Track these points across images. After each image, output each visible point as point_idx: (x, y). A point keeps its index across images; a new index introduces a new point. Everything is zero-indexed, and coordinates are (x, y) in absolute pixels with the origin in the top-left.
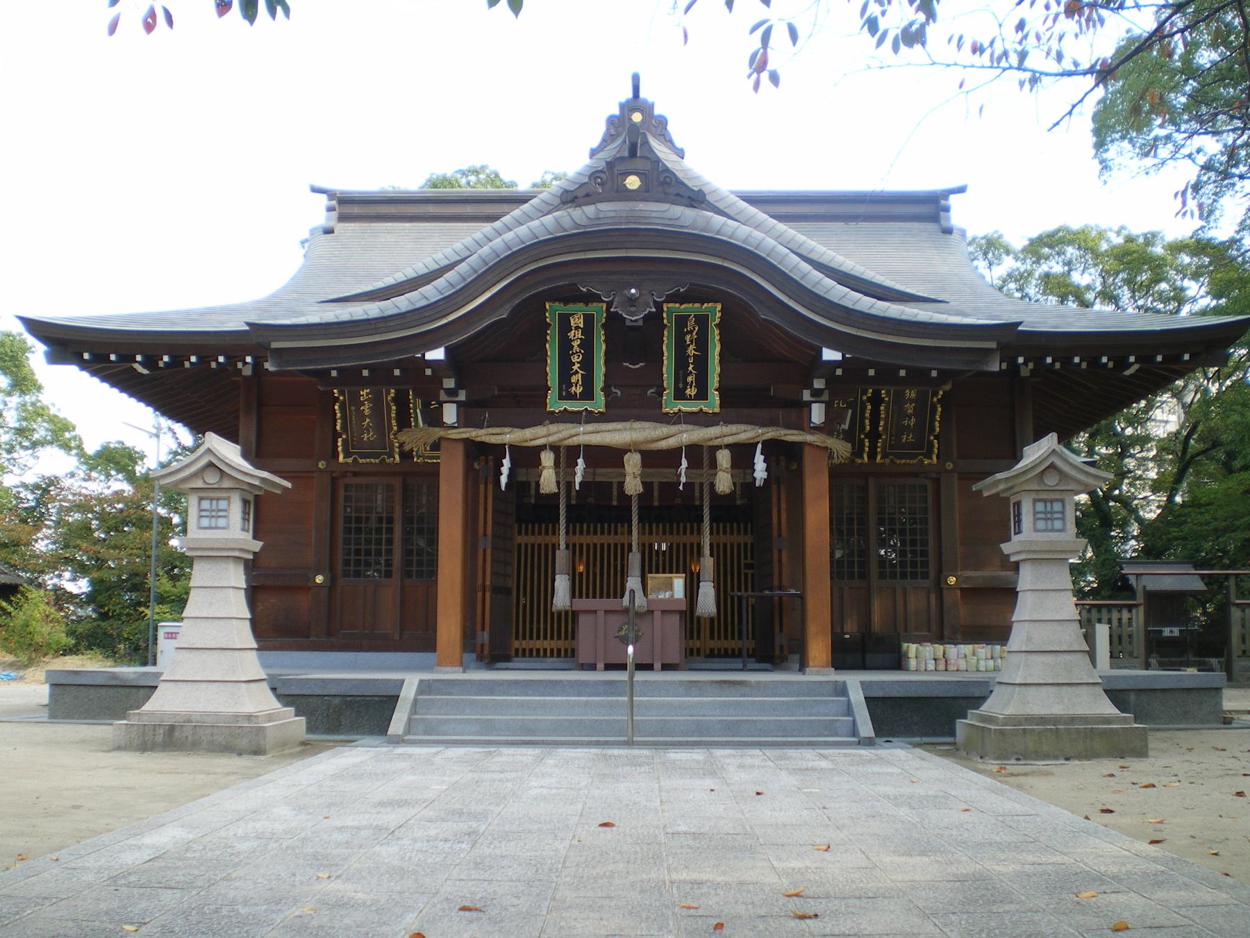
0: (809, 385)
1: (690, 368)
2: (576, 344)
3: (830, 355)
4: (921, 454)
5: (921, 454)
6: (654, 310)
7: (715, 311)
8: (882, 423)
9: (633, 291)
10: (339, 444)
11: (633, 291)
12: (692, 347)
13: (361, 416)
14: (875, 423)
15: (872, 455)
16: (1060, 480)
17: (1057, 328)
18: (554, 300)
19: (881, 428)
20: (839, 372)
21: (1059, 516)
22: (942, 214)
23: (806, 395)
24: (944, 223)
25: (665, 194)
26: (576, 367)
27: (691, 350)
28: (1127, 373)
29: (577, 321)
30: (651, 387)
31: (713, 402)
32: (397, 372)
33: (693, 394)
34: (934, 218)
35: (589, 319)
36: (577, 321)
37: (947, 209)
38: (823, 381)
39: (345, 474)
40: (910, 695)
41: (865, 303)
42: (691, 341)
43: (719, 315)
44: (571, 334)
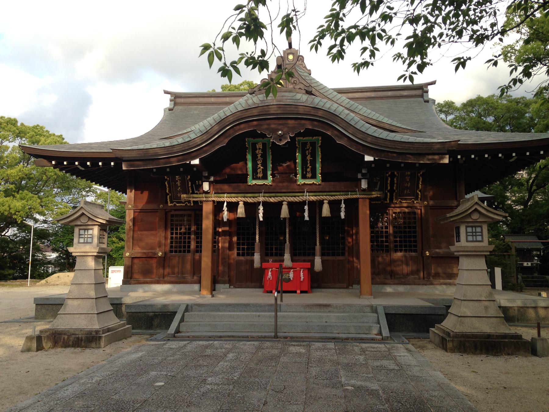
0: (361, 172)
2: (259, 156)
3: (368, 158)
4: (413, 198)
5: (413, 198)
6: (289, 140)
7: (319, 140)
8: (395, 185)
9: (280, 132)
10: (168, 198)
11: (280, 132)
13: (177, 186)
14: (392, 186)
16: (479, 217)
17: (478, 141)
18: (249, 137)
19: (395, 188)
20: (373, 165)
21: (480, 234)
22: (424, 94)
23: (359, 176)
24: (426, 98)
25: (294, 88)
26: (259, 166)
28: (511, 160)
29: (259, 146)
30: (292, 173)
31: (318, 180)
34: (422, 96)
35: (264, 145)
36: (259, 146)
37: (427, 92)
38: (367, 169)
39: (171, 211)
40: (407, 313)
41: (384, 135)
43: (320, 142)
44: (257, 152)
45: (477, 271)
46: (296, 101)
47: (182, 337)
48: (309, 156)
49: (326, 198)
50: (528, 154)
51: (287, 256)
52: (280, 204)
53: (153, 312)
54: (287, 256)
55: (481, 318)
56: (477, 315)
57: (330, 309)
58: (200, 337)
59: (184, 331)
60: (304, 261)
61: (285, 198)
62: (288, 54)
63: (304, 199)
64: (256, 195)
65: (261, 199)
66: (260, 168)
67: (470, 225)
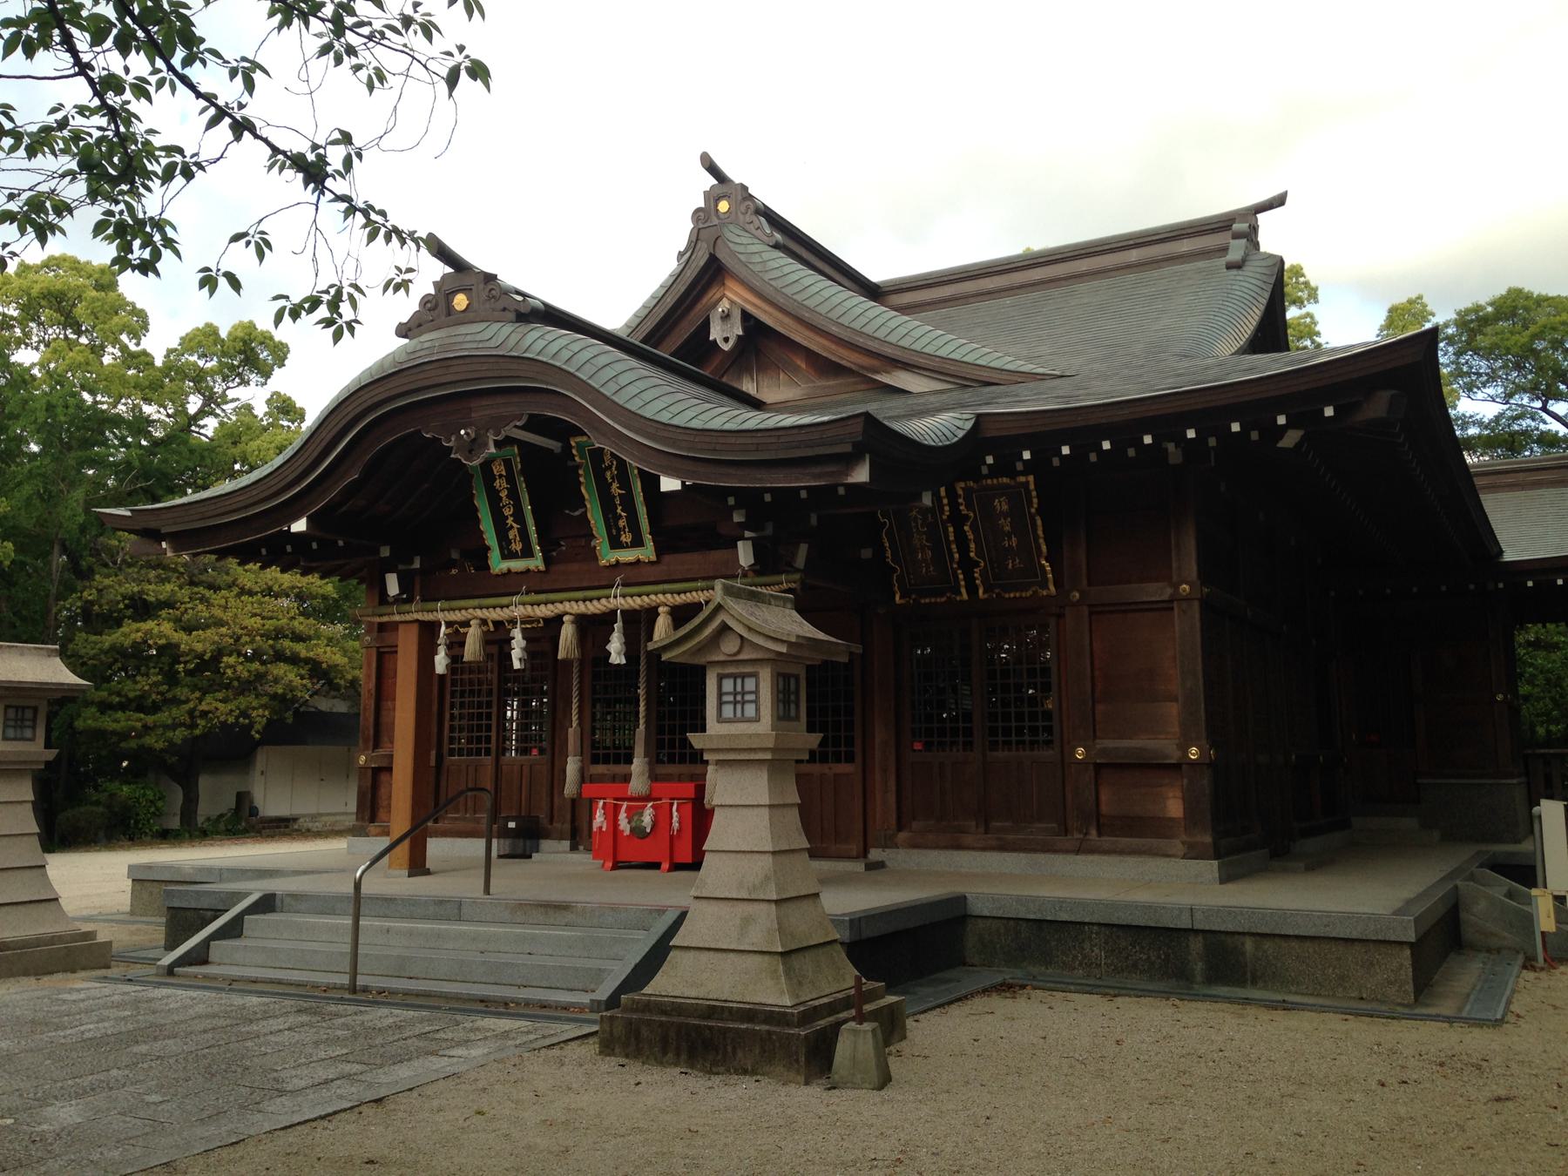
1: (619, 511)
2: (503, 494)
8: (972, 546)
12: (615, 485)
14: (964, 550)
15: (972, 589)
27: (615, 489)
31: (647, 552)
32: (315, 546)
33: (629, 540)
38: (743, 511)
42: (612, 478)
44: (497, 484)
45: (745, 811)
46: (480, 346)
47: (214, 978)
48: (615, 485)
49: (664, 599)
50: (1329, 412)
51: (638, 765)
52: (557, 621)
53: (212, 910)
54: (638, 765)
55: (724, 955)
56: (713, 946)
57: (569, 917)
58: (1266, 1006)
59: (217, 960)
60: (680, 778)
61: (567, 606)
62: (717, 200)
63: (611, 606)
64: (505, 600)
65: (518, 612)
66: (512, 527)
67: (731, 670)
